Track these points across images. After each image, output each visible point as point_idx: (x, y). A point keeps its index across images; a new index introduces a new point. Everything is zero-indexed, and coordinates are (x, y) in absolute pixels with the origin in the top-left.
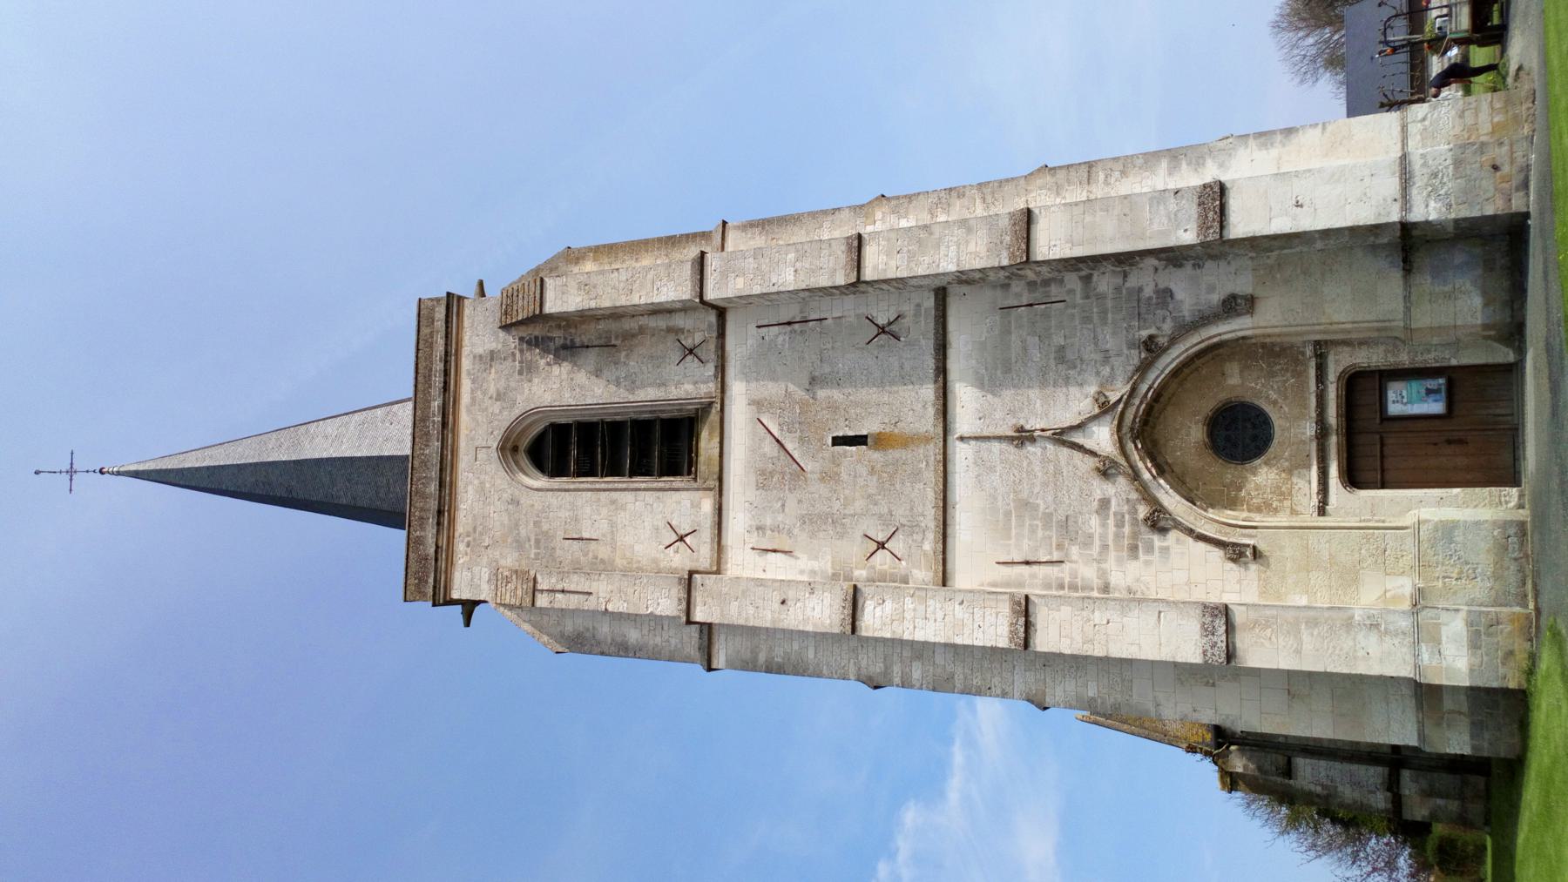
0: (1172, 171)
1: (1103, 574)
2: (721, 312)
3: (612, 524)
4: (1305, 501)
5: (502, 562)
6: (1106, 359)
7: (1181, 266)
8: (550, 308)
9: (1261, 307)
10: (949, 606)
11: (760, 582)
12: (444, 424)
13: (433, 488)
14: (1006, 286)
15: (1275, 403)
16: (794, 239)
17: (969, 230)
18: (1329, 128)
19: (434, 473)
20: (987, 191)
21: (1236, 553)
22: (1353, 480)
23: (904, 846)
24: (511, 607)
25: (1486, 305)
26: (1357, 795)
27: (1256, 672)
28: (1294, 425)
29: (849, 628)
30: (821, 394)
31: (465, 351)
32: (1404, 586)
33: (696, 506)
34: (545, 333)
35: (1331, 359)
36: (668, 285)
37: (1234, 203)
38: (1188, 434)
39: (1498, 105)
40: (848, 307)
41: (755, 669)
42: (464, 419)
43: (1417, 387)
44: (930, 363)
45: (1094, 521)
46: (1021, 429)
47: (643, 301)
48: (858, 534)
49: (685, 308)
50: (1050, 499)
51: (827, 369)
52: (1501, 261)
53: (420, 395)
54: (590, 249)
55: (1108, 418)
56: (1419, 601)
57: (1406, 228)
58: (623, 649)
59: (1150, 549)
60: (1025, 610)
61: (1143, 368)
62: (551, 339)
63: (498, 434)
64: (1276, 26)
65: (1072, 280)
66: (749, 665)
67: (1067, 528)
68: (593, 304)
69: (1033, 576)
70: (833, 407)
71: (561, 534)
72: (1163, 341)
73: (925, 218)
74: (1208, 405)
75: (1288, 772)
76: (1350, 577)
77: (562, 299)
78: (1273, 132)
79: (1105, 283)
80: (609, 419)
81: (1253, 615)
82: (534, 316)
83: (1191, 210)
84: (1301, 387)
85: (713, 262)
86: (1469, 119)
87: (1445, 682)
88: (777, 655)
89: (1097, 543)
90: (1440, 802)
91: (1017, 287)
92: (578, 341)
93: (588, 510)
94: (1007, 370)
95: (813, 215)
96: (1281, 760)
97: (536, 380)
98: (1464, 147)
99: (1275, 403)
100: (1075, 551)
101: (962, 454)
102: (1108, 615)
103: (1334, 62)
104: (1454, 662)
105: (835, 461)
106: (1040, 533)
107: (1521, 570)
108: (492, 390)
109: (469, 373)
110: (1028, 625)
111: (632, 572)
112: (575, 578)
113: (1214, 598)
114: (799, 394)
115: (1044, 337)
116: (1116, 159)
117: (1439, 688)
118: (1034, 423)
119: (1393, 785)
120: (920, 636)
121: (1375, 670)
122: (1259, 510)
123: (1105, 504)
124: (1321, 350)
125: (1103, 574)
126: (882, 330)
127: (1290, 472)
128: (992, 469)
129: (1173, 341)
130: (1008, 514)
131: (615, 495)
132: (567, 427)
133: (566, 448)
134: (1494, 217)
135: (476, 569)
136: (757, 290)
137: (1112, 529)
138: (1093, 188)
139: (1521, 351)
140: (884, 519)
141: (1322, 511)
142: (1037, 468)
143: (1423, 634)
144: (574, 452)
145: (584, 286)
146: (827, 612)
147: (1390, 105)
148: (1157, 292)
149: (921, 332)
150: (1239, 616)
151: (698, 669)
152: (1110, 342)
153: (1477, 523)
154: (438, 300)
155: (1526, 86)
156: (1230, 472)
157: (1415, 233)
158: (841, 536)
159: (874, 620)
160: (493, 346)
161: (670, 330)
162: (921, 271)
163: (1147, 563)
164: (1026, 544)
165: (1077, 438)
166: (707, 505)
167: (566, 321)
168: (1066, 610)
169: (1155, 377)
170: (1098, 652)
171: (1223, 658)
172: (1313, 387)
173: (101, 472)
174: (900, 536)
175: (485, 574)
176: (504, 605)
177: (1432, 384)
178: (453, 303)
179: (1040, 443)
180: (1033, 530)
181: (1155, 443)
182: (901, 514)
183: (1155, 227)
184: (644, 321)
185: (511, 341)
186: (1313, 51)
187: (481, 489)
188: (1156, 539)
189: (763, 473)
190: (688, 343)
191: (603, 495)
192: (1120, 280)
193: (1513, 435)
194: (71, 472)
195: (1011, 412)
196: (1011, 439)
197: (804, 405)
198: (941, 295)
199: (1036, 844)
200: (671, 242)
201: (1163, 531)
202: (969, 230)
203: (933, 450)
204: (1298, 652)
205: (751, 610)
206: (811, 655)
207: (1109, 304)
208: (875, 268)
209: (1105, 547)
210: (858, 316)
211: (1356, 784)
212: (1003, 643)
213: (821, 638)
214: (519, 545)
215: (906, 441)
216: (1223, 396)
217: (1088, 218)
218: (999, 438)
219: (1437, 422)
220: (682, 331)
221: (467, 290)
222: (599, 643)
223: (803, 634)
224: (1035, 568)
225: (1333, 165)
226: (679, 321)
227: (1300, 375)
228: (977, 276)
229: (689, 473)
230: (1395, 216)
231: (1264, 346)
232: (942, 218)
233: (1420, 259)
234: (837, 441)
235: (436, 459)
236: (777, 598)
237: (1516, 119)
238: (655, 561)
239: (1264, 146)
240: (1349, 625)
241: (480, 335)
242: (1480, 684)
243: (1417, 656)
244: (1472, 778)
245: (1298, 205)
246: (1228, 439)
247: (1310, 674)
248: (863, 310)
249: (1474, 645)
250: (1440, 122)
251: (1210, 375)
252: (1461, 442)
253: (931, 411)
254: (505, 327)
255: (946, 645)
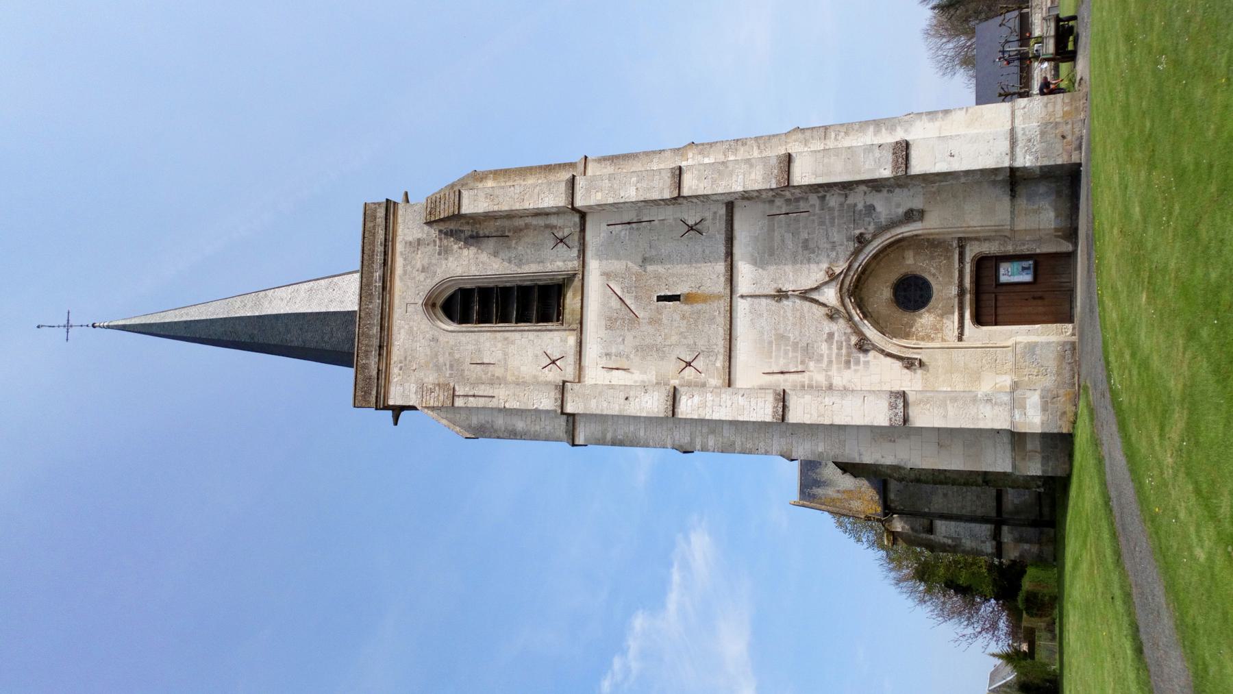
0: (877, 132)
1: (829, 378)
2: (583, 215)
3: (505, 354)
4: (950, 333)
5: (426, 380)
6: (833, 248)
7: (879, 191)
8: (464, 210)
9: (927, 216)
10: (735, 398)
11: (611, 387)
12: (384, 288)
13: (375, 330)
14: (772, 202)
15: (934, 275)
16: (633, 169)
17: (751, 166)
18: (970, 111)
19: (377, 320)
20: (761, 142)
21: (909, 363)
22: (979, 320)
23: (633, 645)
24: (433, 408)
25: (1057, 217)
26: (974, 545)
27: (920, 430)
28: (945, 288)
29: (670, 414)
30: (650, 268)
31: (399, 239)
32: (1006, 381)
33: (564, 341)
34: (457, 226)
35: (968, 249)
36: (551, 198)
37: (914, 154)
38: (881, 294)
39: (1067, 101)
40: (669, 213)
41: (604, 443)
42: (398, 285)
43: (1017, 266)
44: (722, 250)
45: (824, 346)
46: (780, 291)
47: (531, 206)
48: (674, 358)
49: (558, 212)
50: (797, 333)
51: (654, 253)
52: (1066, 191)
53: (365, 268)
54: (491, 172)
55: (834, 283)
56: (1015, 386)
57: (1013, 170)
58: (513, 434)
59: (857, 362)
60: (783, 399)
61: (856, 253)
62: (462, 231)
63: (423, 295)
64: (927, 33)
65: (814, 199)
66: (601, 441)
67: (808, 351)
68: (496, 208)
69: (785, 381)
70: (658, 277)
71: (468, 360)
72: (868, 237)
73: (721, 158)
74: (894, 276)
75: (931, 530)
76: (976, 376)
77: (470, 206)
78: (936, 112)
79: (833, 200)
80: (501, 285)
81: (919, 396)
82: (454, 215)
83: (889, 157)
84: (950, 266)
85: (580, 182)
86: (1050, 108)
87: (1028, 431)
88: (619, 432)
89: (825, 360)
90: (1026, 546)
91: (779, 202)
92: (481, 233)
93: (488, 344)
94: (772, 254)
95: (647, 154)
96: (926, 522)
97: (451, 259)
98: (1046, 124)
99: (934, 275)
100: (812, 364)
101: (742, 306)
102: (833, 399)
103: (967, 61)
104: (1034, 419)
105: (659, 311)
106: (790, 354)
107: (1072, 370)
108: (419, 266)
109: (401, 253)
110: (784, 407)
111: (520, 383)
112: (483, 387)
113: (896, 388)
114: (636, 268)
115: (795, 234)
116: (842, 125)
117: (1025, 434)
118: (788, 287)
119: (997, 536)
120: (716, 417)
121: (989, 425)
122: (923, 339)
123: (831, 335)
124: (962, 243)
125: (829, 378)
126: (691, 228)
127: (942, 316)
128: (761, 315)
129: (875, 236)
130: (770, 343)
131: (506, 334)
132: (471, 290)
133: (467, 305)
134: (1062, 166)
135: (407, 385)
136: (611, 201)
137: (835, 350)
138: (828, 142)
139: (1076, 245)
140: (691, 348)
141: (960, 339)
142: (789, 314)
143: (1016, 403)
144: (476, 307)
145: (490, 196)
146: (656, 404)
147: (1006, 96)
148: (865, 207)
149: (717, 229)
150: (911, 398)
151: (566, 446)
152: (836, 237)
153: (1048, 343)
154: (379, 204)
155: (1084, 89)
156: (906, 317)
157: (1018, 174)
158: (662, 359)
159: (687, 408)
160: (420, 236)
161: (547, 226)
162: (720, 191)
163: (856, 371)
164: (782, 361)
165: (815, 296)
166: (572, 340)
167: (474, 219)
168: (808, 398)
169: (863, 258)
170: (827, 422)
171: (901, 422)
172: (957, 265)
173: (94, 326)
174: (701, 358)
175: (413, 388)
176: (428, 408)
177: (1025, 264)
178: (390, 206)
179: (792, 299)
180: (786, 353)
181: (861, 299)
182: (702, 344)
183: (867, 167)
184: (528, 220)
185: (433, 232)
186: (951, 53)
187: (410, 332)
188: (862, 356)
189: (610, 319)
190: (560, 235)
191: (498, 335)
192: (843, 199)
193: (1070, 293)
194: (68, 326)
195: (774, 280)
196: (773, 297)
197: (638, 275)
198: (730, 206)
199: (733, 643)
200: (549, 169)
201: (866, 351)
202: (751, 166)
203: (723, 304)
204: (945, 417)
205: (605, 404)
206: (642, 433)
207: (836, 213)
208: (690, 188)
209: (830, 362)
210: (675, 219)
211: (973, 536)
212: (769, 419)
213: (651, 421)
214: (438, 368)
215: (706, 298)
216: (903, 271)
217: (826, 160)
218: (766, 296)
219: (1026, 288)
220: (555, 227)
221: (398, 198)
222: (496, 431)
223: (636, 418)
224: (787, 376)
225: (971, 133)
226: (553, 220)
227: (949, 258)
228: (755, 194)
229: (558, 320)
230: (1006, 163)
231: (928, 240)
232: (732, 158)
233: (1021, 190)
234: (660, 299)
235: (377, 312)
236: (623, 396)
237: (1076, 108)
238: (535, 377)
239: (931, 120)
240: (975, 400)
241: (409, 228)
242: (1047, 431)
243: (1012, 416)
244: (1046, 530)
245: (952, 156)
246: (905, 297)
247: (952, 429)
248: (679, 215)
249: (1044, 409)
250: (1032, 111)
251: (896, 257)
252: (1041, 298)
253: (722, 279)
254: (429, 223)
255: (731, 422)
